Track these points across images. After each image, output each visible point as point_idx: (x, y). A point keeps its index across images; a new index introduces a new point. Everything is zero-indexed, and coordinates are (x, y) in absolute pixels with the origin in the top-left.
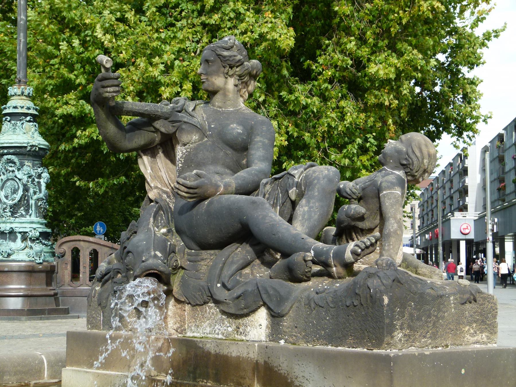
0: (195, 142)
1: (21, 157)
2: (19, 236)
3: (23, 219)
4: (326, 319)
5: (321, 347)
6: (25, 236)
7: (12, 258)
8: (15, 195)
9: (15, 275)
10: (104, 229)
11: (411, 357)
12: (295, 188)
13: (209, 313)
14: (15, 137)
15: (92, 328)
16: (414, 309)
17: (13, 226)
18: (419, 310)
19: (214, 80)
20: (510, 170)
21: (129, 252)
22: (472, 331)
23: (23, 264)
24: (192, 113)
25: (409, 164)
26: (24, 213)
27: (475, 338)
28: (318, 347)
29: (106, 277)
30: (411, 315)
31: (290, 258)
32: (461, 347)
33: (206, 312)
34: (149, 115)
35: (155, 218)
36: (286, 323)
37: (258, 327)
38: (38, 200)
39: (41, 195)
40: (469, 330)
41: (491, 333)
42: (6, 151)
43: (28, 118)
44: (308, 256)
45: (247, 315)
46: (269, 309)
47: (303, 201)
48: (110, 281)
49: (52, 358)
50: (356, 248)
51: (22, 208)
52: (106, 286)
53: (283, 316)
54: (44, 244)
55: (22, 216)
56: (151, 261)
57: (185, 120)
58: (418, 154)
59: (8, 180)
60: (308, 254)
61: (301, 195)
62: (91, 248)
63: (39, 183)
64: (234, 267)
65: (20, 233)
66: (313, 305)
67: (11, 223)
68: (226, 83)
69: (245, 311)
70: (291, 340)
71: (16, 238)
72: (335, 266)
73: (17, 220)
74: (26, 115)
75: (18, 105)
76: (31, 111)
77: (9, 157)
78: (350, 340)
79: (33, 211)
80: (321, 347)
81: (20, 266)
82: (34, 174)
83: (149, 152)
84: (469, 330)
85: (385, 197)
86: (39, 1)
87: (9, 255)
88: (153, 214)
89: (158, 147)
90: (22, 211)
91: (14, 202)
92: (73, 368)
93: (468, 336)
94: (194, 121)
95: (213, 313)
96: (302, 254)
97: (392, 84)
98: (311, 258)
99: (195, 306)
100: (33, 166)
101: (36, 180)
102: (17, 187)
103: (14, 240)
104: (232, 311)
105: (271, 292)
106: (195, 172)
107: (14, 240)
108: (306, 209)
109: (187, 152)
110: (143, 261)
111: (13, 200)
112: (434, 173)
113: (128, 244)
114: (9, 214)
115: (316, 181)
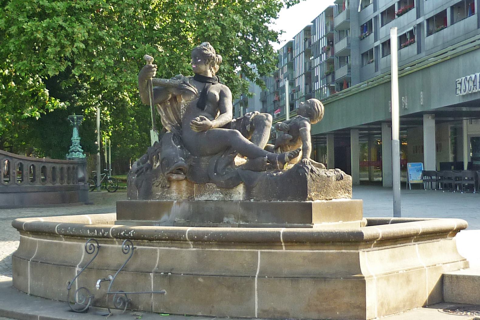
0: (192, 100)
12: (249, 125)
13: (209, 188)
19: (200, 66)
27: (342, 196)
33: (207, 188)
35: (173, 140)
37: (238, 194)
44: (265, 159)
50: (291, 155)
52: (140, 177)
56: (180, 162)
60: (265, 158)
62: (41, 166)
64: (224, 165)
70: (257, 199)
78: (289, 198)
86: (253, 1)
88: (172, 138)
95: (211, 188)
96: (262, 158)
97: (25, 96)
98: (266, 160)
109: (187, 105)
115: (261, 122)
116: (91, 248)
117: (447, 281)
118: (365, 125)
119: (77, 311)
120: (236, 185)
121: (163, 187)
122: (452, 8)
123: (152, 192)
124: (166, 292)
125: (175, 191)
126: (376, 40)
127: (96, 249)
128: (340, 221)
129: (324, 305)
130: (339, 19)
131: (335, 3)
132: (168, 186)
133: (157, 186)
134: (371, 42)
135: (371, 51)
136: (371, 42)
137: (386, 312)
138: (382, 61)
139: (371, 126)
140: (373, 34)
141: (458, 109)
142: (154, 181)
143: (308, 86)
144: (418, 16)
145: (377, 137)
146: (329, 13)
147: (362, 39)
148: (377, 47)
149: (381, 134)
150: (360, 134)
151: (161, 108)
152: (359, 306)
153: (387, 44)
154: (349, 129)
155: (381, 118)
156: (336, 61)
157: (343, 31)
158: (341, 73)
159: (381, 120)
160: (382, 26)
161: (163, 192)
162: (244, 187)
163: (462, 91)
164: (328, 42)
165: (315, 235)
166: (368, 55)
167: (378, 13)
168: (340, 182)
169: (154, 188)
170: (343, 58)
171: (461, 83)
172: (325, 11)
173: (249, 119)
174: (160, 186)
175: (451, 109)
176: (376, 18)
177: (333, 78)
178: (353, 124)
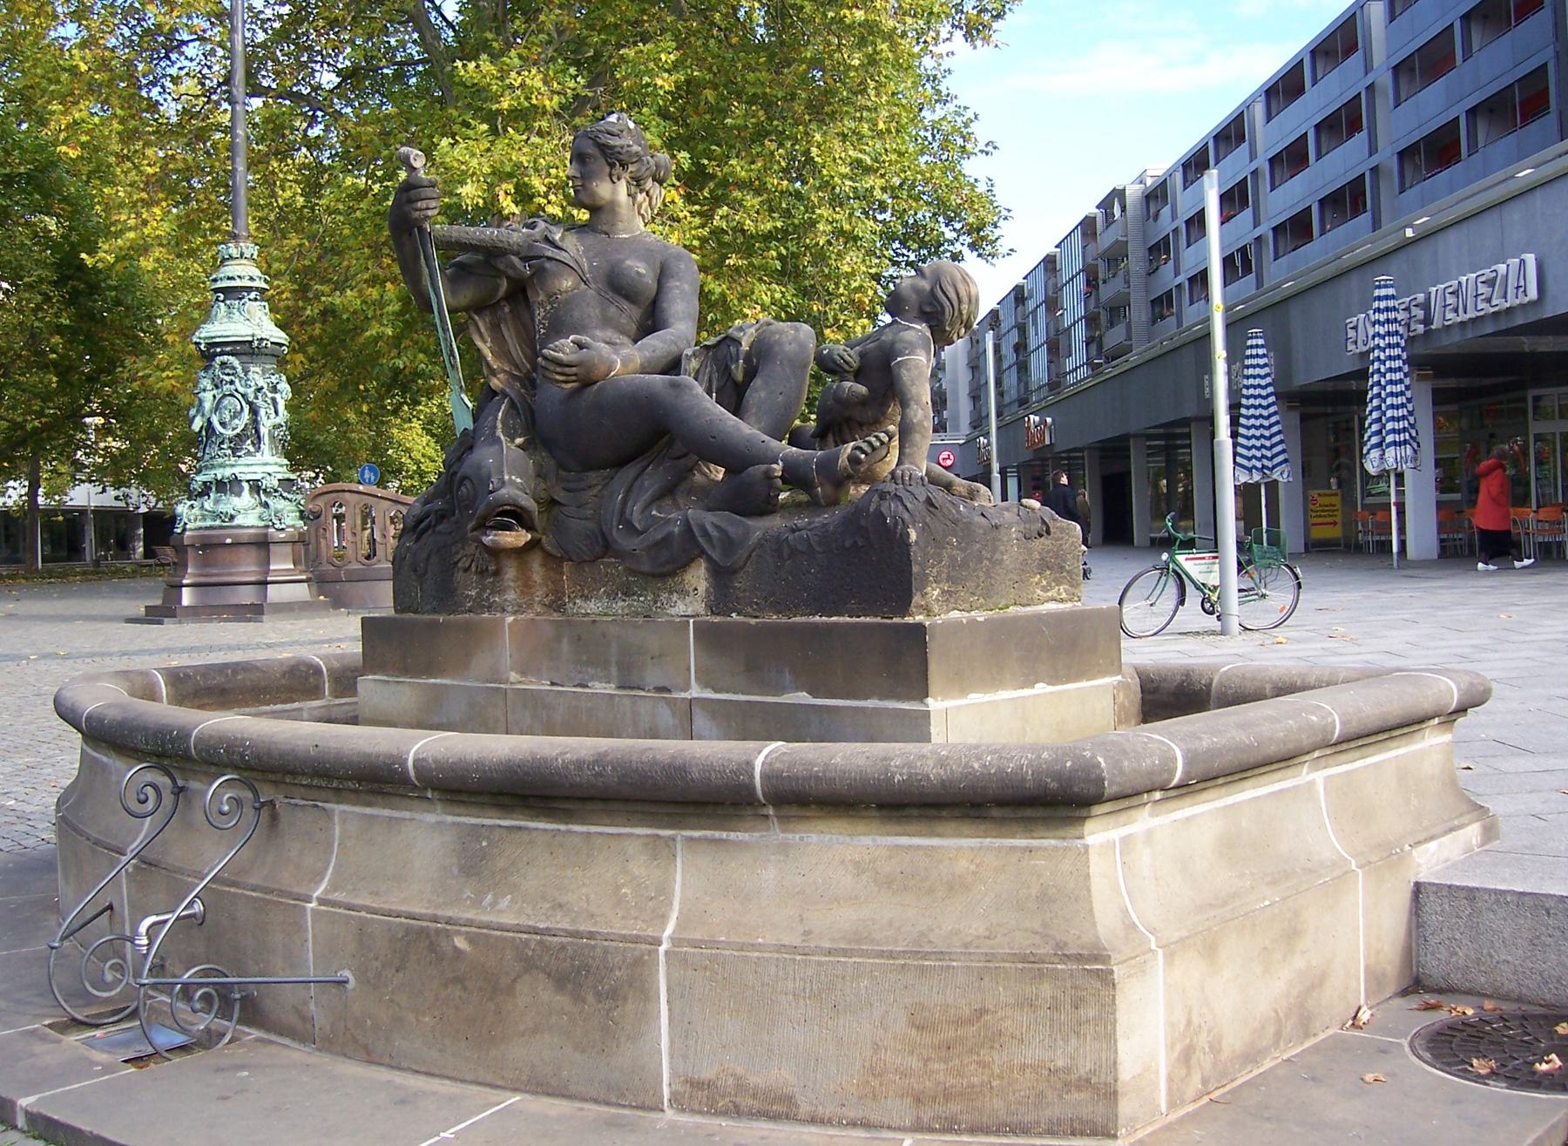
1: (245, 358)
2: (246, 485)
3: (250, 460)
4: (809, 572)
5: (804, 619)
6: (256, 487)
7: (236, 522)
8: (236, 421)
9: (243, 549)
10: (375, 475)
11: (958, 624)
14: (232, 326)
15: (403, 611)
16: (958, 548)
17: (236, 470)
18: (963, 550)
20: (1010, 367)
21: (464, 478)
22: (1044, 583)
23: (252, 531)
24: (560, 244)
25: (937, 312)
26: (251, 449)
27: (1050, 594)
28: (798, 619)
29: (423, 525)
30: (952, 558)
31: (743, 475)
32: (1028, 609)
34: (486, 248)
36: (740, 583)
38: (275, 427)
39: (279, 420)
40: (1040, 581)
41: (1072, 586)
42: (218, 350)
43: (253, 295)
45: (673, 574)
46: (709, 560)
47: (758, 382)
48: (430, 532)
49: (336, 665)
51: (249, 442)
53: (735, 572)
54: (285, 498)
55: (249, 453)
57: (549, 254)
58: (953, 295)
59: (225, 396)
60: (775, 466)
61: (751, 373)
63: (274, 400)
65: (248, 481)
66: (786, 552)
67: (232, 466)
68: (614, 192)
69: (669, 567)
71: (242, 489)
72: (822, 485)
73: (242, 461)
74: (249, 289)
75: (235, 274)
76: (257, 284)
77: (225, 358)
79: (265, 446)
80: (804, 619)
81: (250, 535)
82: (265, 386)
83: (488, 312)
84: (1040, 581)
85: (900, 367)
87: (232, 518)
89: (503, 303)
90: (248, 445)
91: (235, 432)
92: (377, 677)
93: (1039, 591)
94: (561, 256)
96: (763, 467)
99: (579, 563)
100: (264, 372)
101: (270, 395)
102: (239, 407)
103: (239, 494)
104: (646, 568)
105: (714, 533)
106: (571, 337)
107: (239, 494)
108: (763, 394)
110: (492, 492)
111: (234, 429)
112: (1031, 297)
113: (460, 468)
114: (229, 452)
116: (142, 797)
117: (1431, 904)
118: (1156, 427)
119: (93, 1021)
120: (685, 565)
121: (482, 573)
122: (1322, 202)
123: (456, 589)
124: (351, 979)
125: (512, 584)
126: (1177, 274)
127: (168, 800)
128: (1037, 686)
129: (938, 1072)
130: (1106, 240)
131: (1098, 207)
132: (492, 568)
133: (467, 570)
134: (1168, 278)
135: (1169, 294)
136: (1168, 278)
137: (1205, 1082)
138: (1191, 313)
139: (1171, 431)
140: (1171, 262)
141: (1342, 386)
142: (457, 553)
143: (1053, 365)
144: (1256, 224)
145: (1183, 454)
146: (1087, 225)
147: (1152, 272)
148: (1179, 286)
149: (1189, 446)
150: (1149, 447)
151: (481, 324)
152: (1088, 1081)
153: (1202, 278)
154: (1125, 438)
155: (1189, 411)
156: (1104, 318)
157: (1114, 257)
158: (1114, 337)
159: (1189, 415)
160: (1189, 245)
161: (483, 590)
162: (707, 569)
163: (1360, 342)
164: (1088, 283)
165: (898, 777)
166: (1162, 304)
167: (1182, 278)
168: (1038, 544)
169: (459, 576)
170: (1117, 310)
171: (1355, 328)
172: (1080, 224)
173: (738, 343)
174: (473, 569)
175: (1330, 387)
176: (1176, 231)
177: (1100, 347)
178: (1133, 427)
